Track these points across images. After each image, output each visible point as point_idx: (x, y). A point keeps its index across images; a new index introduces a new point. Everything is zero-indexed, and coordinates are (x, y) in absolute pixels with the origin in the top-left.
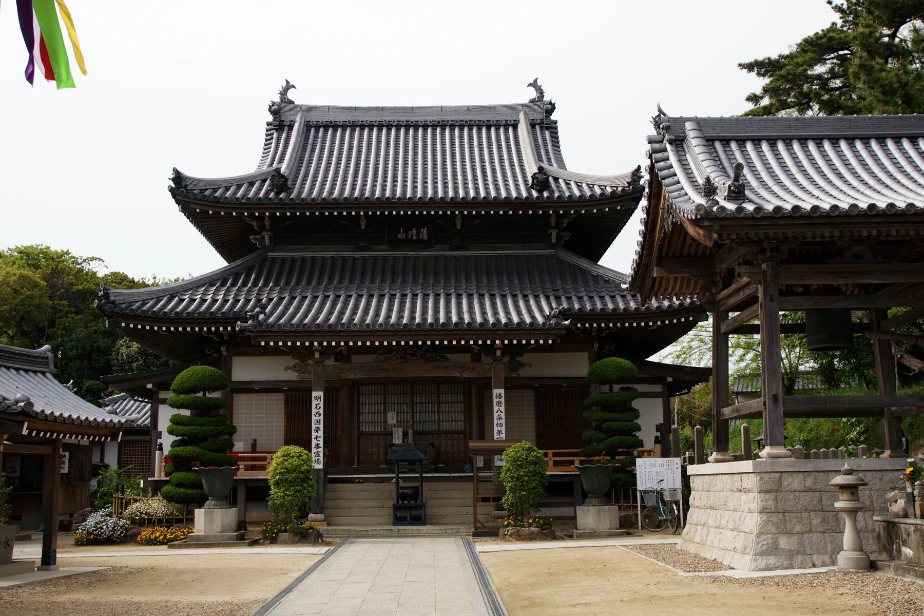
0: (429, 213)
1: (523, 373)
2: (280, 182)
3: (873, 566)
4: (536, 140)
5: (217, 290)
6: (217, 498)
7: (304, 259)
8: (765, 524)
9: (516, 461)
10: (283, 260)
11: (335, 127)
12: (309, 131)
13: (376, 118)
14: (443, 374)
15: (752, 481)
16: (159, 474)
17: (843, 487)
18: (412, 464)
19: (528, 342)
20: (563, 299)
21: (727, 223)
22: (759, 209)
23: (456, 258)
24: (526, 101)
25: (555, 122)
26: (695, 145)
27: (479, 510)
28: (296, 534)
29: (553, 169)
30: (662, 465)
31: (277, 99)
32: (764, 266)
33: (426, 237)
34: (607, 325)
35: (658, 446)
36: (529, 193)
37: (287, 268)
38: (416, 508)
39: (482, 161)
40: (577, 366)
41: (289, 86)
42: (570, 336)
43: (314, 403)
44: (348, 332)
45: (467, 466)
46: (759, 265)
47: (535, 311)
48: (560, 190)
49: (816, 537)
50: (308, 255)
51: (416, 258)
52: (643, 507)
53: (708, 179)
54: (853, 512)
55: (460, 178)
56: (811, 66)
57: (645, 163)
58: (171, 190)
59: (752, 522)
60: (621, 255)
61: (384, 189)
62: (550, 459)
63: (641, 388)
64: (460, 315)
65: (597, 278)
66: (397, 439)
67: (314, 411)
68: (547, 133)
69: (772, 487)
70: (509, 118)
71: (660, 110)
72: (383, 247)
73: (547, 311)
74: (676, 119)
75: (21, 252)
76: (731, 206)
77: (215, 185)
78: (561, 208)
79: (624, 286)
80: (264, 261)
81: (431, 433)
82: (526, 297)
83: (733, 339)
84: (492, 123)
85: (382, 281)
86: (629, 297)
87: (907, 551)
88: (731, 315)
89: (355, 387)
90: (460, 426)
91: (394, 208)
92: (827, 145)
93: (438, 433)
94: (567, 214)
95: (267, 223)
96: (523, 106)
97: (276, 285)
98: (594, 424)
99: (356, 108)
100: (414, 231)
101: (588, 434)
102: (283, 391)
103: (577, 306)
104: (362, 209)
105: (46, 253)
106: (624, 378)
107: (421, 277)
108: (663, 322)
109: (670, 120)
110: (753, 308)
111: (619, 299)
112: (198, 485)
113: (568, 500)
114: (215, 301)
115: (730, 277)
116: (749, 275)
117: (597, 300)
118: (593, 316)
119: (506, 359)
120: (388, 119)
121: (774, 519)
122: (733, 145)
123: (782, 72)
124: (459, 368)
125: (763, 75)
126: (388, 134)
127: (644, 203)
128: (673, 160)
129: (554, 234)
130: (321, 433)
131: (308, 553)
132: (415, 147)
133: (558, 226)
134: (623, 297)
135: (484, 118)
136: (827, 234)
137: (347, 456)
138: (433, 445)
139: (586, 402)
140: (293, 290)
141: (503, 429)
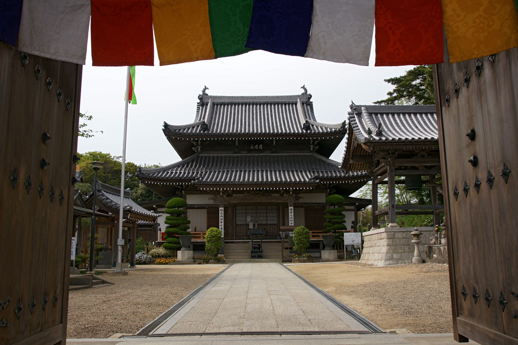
0: (263, 139)
1: (301, 201)
2: (205, 127)
3: (424, 262)
4: (304, 110)
5: (181, 169)
6: (186, 247)
7: (214, 157)
8: (388, 250)
9: (298, 233)
10: (206, 157)
11: (224, 105)
12: (214, 106)
13: (241, 101)
14: (270, 201)
15: (384, 235)
16: (159, 240)
17: (414, 235)
18: (256, 235)
19: (303, 188)
20: (316, 172)
21: (376, 144)
22: (387, 139)
23: (274, 157)
24: (300, 94)
25: (312, 102)
26: (365, 115)
27: (284, 253)
28: (216, 260)
29: (311, 121)
30: (354, 235)
31: (201, 93)
32: (389, 159)
33: (261, 148)
34: (333, 182)
35: (353, 229)
36: (302, 131)
37: (207, 160)
38: (259, 252)
39: (283, 118)
40: (321, 198)
41: (206, 88)
42: (317, 187)
43: (220, 212)
44: (234, 184)
45: (278, 237)
46: (388, 159)
47: (306, 177)
48: (314, 130)
49: (406, 254)
50: (215, 155)
51: (258, 156)
52: (346, 252)
53: (369, 129)
54: (418, 244)
55: (275, 125)
56: (413, 81)
57: (347, 122)
58: (163, 130)
59: (384, 249)
60: (338, 155)
61: (245, 129)
62: (311, 234)
63: (347, 207)
64: (276, 178)
65: (329, 164)
66: (251, 227)
67: (220, 215)
68: (309, 107)
69: (391, 236)
70: (293, 101)
71: (352, 103)
72: (245, 152)
73: (310, 177)
74: (358, 106)
75: (90, 154)
76: (377, 138)
77: (180, 128)
78: (315, 137)
79: (340, 167)
80: (198, 158)
81: (264, 225)
82: (293, 171)
83: (379, 186)
84: (287, 102)
85: (245, 165)
86: (341, 172)
87: (435, 256)
88: (379, 177)
89: (235, 206)
90: (275, 222)
91: (249, 137)
92: (412, 116)
93: (267, 225)
94: (317, 139)
95: (199, 143)
96: (299, 96)
97: (204, 167)
98: (328, 220)
99: (232, 97)
100: (257, 146)
101: (325, 224)
102: (206, 208)
103: (321, 175)
104: (237, 137)
105: (100, 154)
106: (340, 204)
107: (260, 164)
108: (354, 181)
109: (356, 106)
110: (386, 174)
111: (337, 172)
112: (179, 243)
113: (318, 250)
114: (176, 173)
115: (378, 163)
116: (384, 162)
117: (329, 172)
118: (327, 179)
119: (294, 195)
120: (245, 101)
121: (392, 248)
122: (379, 115)
123: (401, 84)
124: (275, 199)
125: (394, 84)
126: (246, 107)
127: (346, 136)
128: (357, 121)
129: (312, 147)
130: (223, 224)
131: (220, 267)
132: (256, 112)
133: (313, 143)
134: (339, 171)
135: (284, 101)
136: (411, 148)
137: (233, 233)
138: (265, 229)
139: (325, 212)
140: (210, 169)
141: (293, 222)
